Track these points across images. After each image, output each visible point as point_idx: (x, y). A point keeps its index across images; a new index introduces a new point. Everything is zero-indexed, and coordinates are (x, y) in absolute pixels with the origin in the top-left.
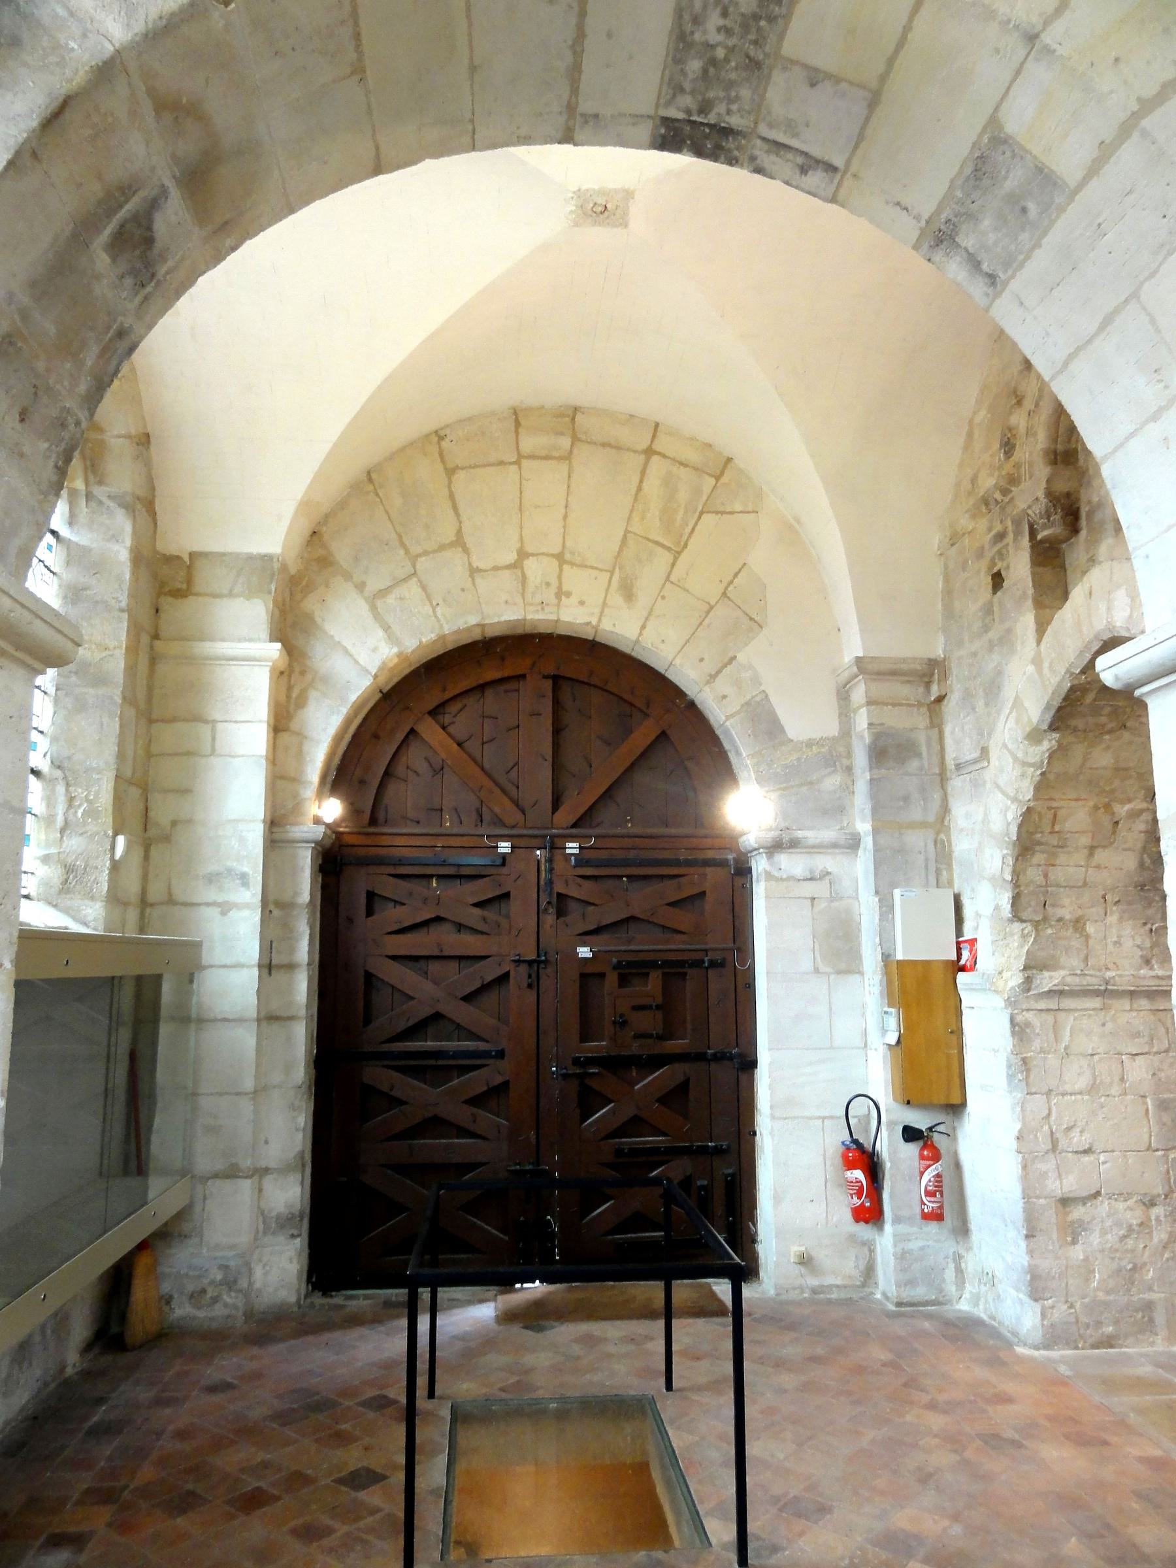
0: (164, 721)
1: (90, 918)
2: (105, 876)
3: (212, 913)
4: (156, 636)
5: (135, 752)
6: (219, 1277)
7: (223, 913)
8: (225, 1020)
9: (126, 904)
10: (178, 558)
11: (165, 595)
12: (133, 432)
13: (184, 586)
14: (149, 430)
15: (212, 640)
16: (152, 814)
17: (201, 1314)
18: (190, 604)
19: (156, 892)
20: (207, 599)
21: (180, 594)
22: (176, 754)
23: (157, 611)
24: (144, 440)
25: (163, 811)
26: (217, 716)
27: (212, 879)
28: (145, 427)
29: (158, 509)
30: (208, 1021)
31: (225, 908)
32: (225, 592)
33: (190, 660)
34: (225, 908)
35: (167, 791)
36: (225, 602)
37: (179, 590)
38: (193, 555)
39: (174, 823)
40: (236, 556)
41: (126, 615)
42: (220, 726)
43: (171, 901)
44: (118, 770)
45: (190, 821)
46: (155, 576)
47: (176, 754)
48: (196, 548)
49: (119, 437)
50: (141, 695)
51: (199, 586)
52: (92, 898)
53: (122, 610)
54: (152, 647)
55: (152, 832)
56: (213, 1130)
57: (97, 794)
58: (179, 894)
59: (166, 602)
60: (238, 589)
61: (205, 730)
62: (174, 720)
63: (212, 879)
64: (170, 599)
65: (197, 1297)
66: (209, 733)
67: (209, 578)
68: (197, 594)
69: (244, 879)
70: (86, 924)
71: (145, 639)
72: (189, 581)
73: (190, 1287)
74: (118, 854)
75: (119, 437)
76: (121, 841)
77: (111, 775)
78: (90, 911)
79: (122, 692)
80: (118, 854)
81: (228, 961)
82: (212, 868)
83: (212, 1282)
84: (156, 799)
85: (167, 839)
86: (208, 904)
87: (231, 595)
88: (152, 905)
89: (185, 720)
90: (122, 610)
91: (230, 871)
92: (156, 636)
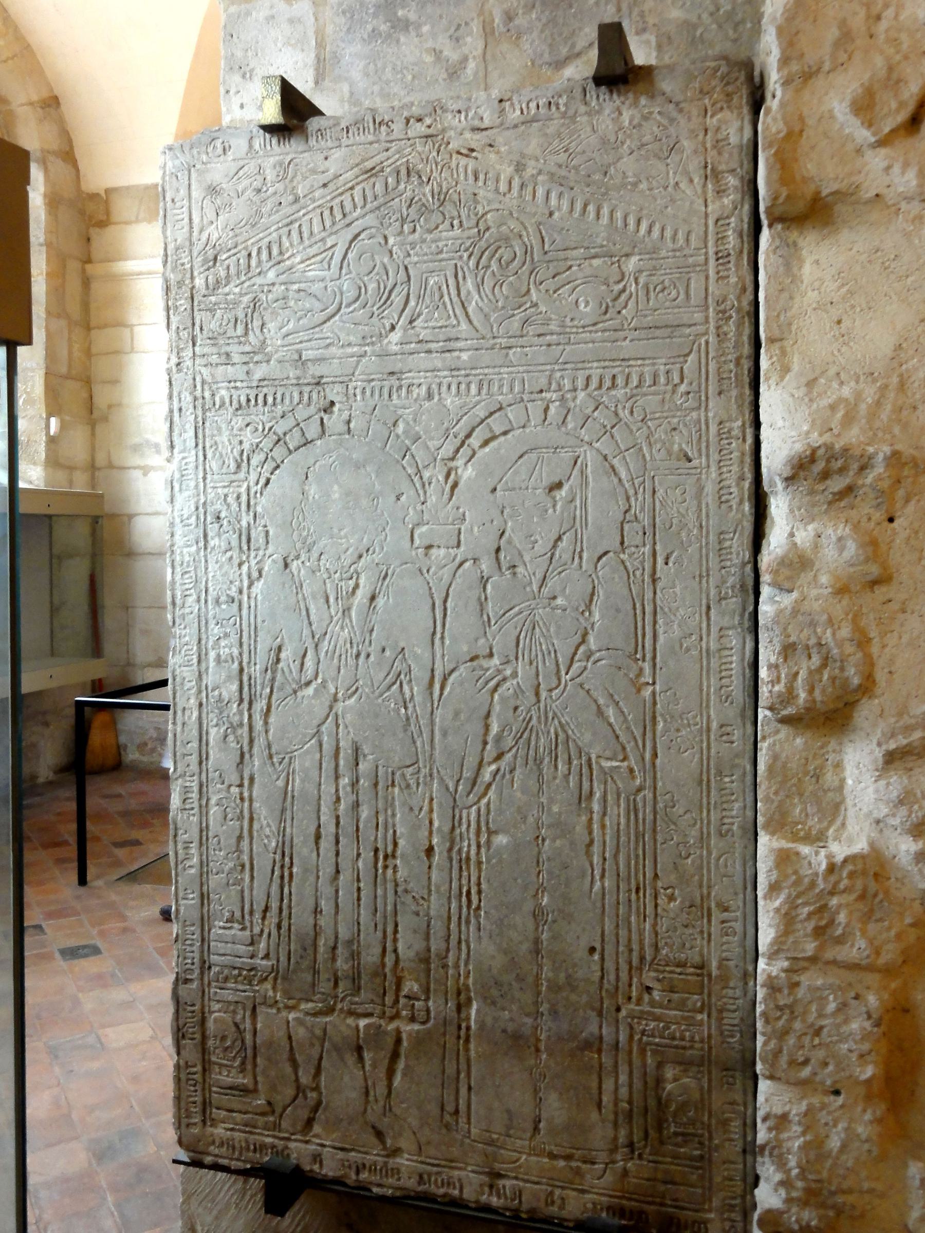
0: (99, 328)
1: (34, 478)
2: (42, 448)
3: (137, 474)
4: (89, 261)
5: (70, 353)
6: (155, 735)
7: (145, 474)
8: (150, 554)
9: (71, 469)
10: (98, 195)
11: (93, 226)
12: (35, 98)
13: (104, 218)
14: (56, 92)
15: (126, 260)
16: (95, 399)
17: (145, 759)
18: (111, 230)
19: (101, 460)
20: (123, 226)
21: (103, 224)
22: (108, 354)
23: (89, 239)
24: (52, 103)
25: (101, 401)
26: (134, 321)
27: (136, 448)
28: (52, 90)
29: (78, 156)
30: (140, 554)
31: (146, 470)
32: (133, 219)
33: (118, 279)
34: (146, 470)
35: (104, 382)
36: (134, 225)
37: (102, 221)
38: (107, 191)
39: (110, 407)
40: (136, 187)
41: (44, 249)
42: (136, 329)
43: (111, 466)
44: (47, 368)
45: (120, 405)
46: (82, 212)
47: (108, 354)
48: (111, 184)
49: (23, 105)
50: (74, 308)
51: (115, 218)
52: (35, 464)
53: (41, 245)
54: (84, 271)
55: (96, 414)
56: (146, 632)
57: (33, 386)
58: (116, 462)
59: (93, 232)
60: (142, 215)
61: (126, 331)
62: (106, 326)
63: (136, 448)
64: (97, 230)
65: (142, 747)
66: (129, 334)
67: (123, 208)
68: (115, 223)
69: (157, 446)
70: (31, 483)
71: (74, 266)
72: (108, 213)
73: (138, 741)
74: (53, 431)
75: (23, 105)
76: (53, 421)
77: (42, 372)
78: (33, 473)
79: (46, 309)
80: (53, 431)
81: (149, 510)
82: (136, 440)
83: (151, 738)
84: (97, 389)
85: (105, 419)
86: (135, 468)
87: (137, 221)
88: (99, 469)
89: (114, 326)
90: (41, 245)
91: (147, 441)
92: (89, 261)
